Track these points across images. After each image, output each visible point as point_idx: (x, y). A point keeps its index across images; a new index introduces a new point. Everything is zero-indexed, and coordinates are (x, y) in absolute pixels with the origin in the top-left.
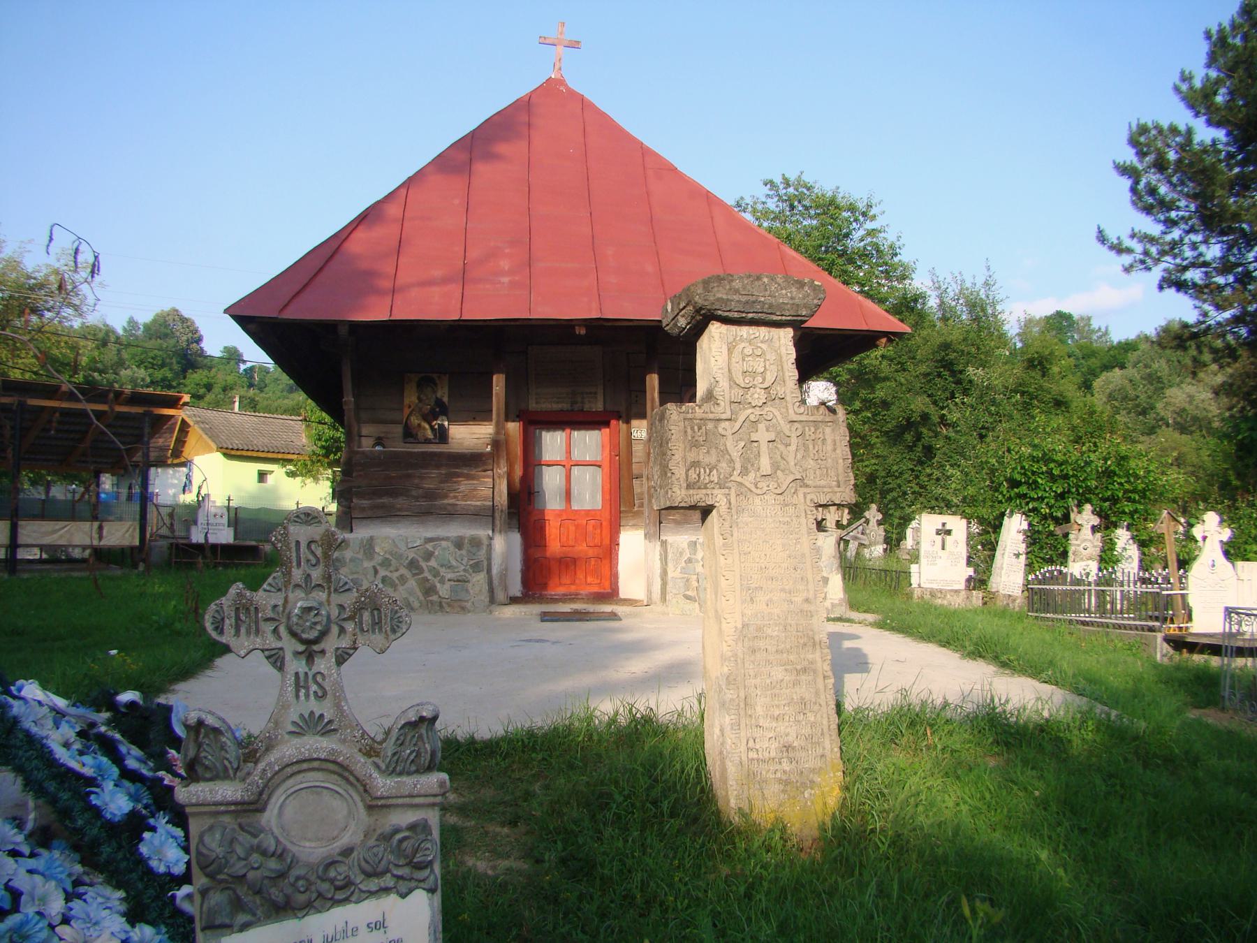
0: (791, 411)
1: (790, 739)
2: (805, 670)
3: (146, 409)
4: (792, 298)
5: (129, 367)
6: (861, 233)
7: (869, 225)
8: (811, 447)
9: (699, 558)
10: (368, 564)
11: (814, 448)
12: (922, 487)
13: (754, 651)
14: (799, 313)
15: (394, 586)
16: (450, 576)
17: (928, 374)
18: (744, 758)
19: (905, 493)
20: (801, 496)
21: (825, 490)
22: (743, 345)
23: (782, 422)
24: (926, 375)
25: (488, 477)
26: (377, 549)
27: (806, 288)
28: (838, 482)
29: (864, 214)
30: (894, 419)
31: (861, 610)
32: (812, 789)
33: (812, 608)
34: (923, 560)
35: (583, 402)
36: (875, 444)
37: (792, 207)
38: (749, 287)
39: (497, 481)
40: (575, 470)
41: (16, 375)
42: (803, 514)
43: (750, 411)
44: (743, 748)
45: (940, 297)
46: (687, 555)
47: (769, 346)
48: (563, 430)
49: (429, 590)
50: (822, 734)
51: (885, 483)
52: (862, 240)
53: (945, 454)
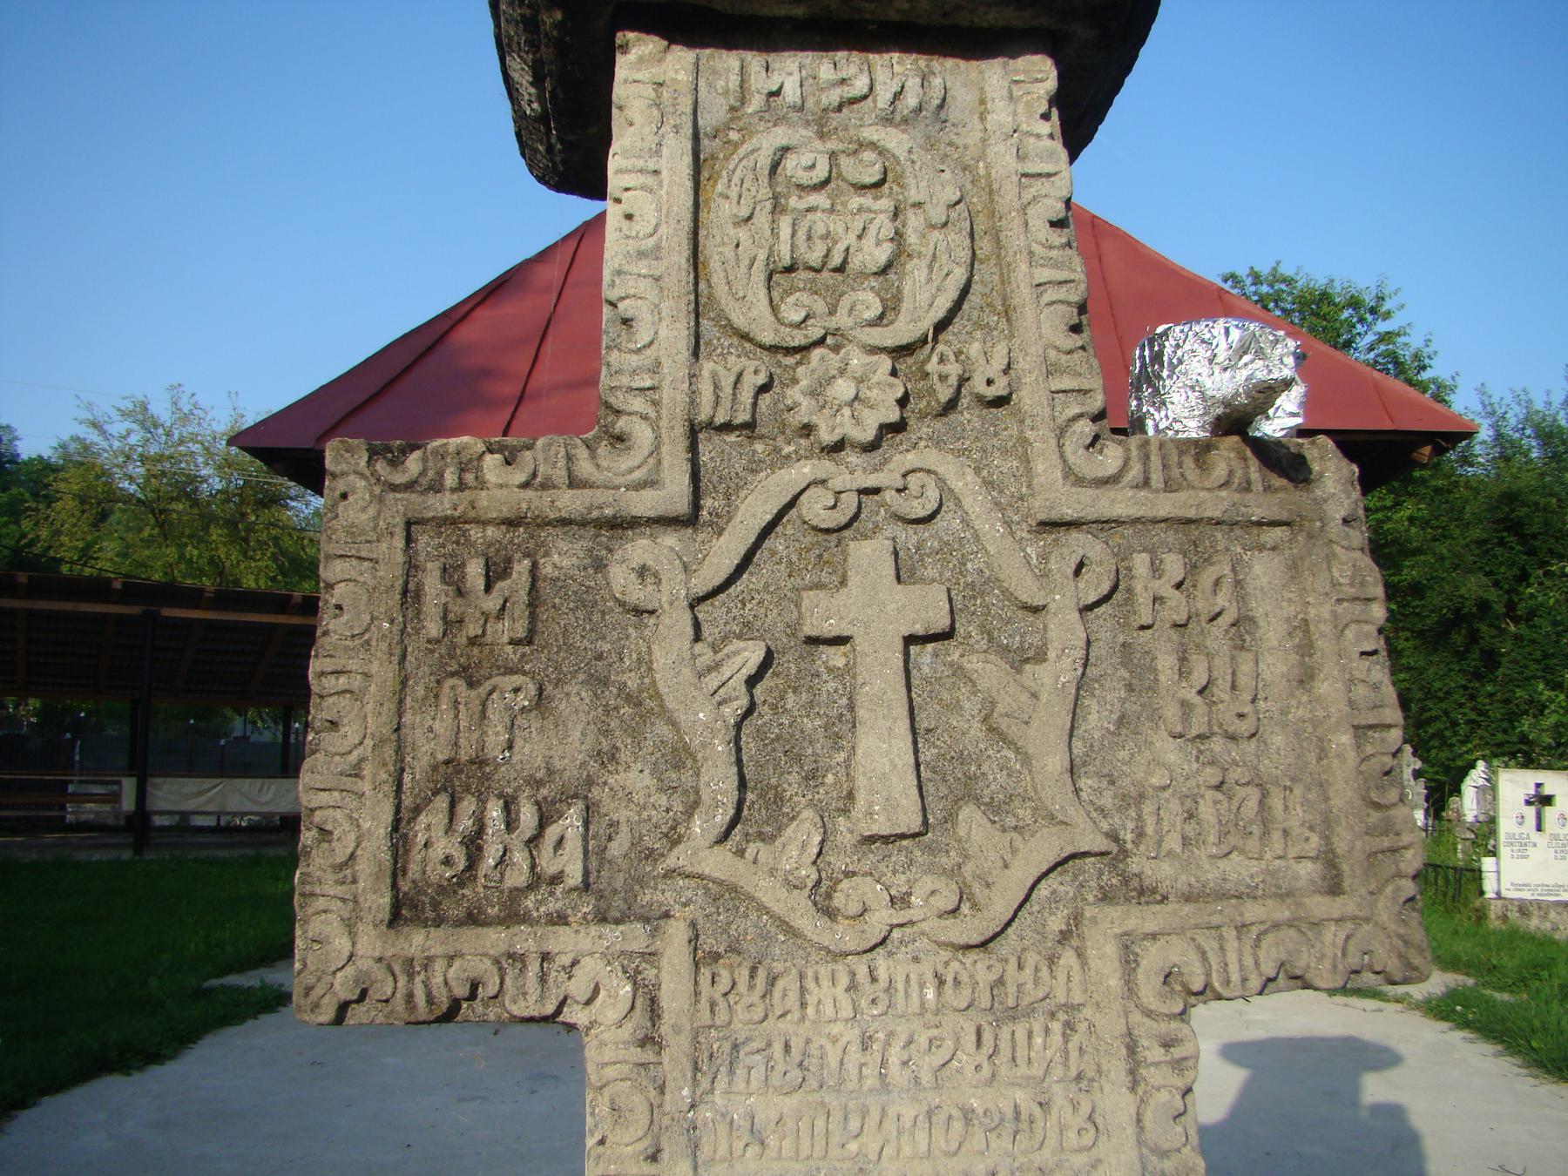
0: (1046, 469)
6: (1370, 338)
7: (1382, 327)
8: (1166, 663)
11: (1183, 672)
12: (1481, 713)
17: (1484, 542)
19: (1455, 724)
22: (781, 136)
23: (991, 528)
24: (1481, 543)
28: (1329, 860)
29: (1373, 311)
30: (1433, 611)
34: (1504, 851)
36: (1403, 649)
41: (249, 583)
42: (1117, 1068)
43: (806, 470)
45: (1495, 426)
51: (1423, 710)
52: (1371, 349)
53: (1515, 662)
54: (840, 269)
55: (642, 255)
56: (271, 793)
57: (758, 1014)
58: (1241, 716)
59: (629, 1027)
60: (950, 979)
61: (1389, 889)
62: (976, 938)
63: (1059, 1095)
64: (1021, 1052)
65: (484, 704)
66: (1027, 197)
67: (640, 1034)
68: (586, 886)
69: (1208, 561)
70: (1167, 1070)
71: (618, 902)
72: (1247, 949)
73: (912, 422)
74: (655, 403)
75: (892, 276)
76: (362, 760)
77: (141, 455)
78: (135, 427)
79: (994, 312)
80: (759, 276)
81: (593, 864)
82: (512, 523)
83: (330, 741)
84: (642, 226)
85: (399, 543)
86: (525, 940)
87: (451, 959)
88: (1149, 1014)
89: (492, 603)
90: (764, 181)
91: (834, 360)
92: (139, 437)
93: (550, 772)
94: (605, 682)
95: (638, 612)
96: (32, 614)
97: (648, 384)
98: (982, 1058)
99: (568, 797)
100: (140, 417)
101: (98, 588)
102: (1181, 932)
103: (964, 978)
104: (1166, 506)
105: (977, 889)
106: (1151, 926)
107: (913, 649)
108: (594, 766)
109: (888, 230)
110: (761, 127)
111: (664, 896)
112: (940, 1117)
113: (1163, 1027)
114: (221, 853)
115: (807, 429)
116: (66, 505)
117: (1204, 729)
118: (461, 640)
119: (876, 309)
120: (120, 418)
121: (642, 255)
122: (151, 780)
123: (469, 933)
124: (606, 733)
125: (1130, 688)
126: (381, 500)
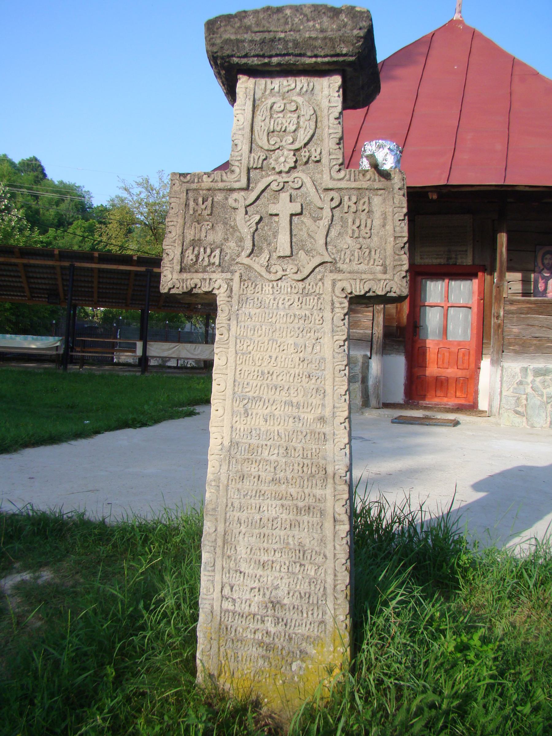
0: (326, 177)
2: (309, 509)
4: (322, 31)
9: (529, 381)
14: (338, 51)
18: (216, 608)
20: (328, 283)
21: (364, 276)
22: (273, 100)
23: (312, 190)
25: (369, 312)
27: (343, 17)
28: (384, 266)
32: (303, 661)
33: (327, 429)
35: (456, 258)
38: (264, 22)
39: (376, 315)
40: (451, 311)
42: (329, 307)
44: (217, 595)
46: (519, 378)
48: (443, 280)
50: (325, 594)
54: (285, 131)
55: (240, 129)
56: (199, 350)
57: (252, 292)
58: (367, 233)
59: (226, 293)
60: (293, 287)
61: (398, 273)
62: (300, 279)
63: (315, 313)
64: (308, 303)
65: (201, 228)
66: (330, 112)
67: (228, 295)
68: (219, 265)
69: (363, 198)
70: (340, 309)
71: (226, 269)
72: (362, 284)
73: (298, 167)
74: (241, 163)
75: (296, 133)
76: (176, 239)
77: (146, 203)
78: (144, 190)
79: (320, 140)
80: (266, 133)
81: (221, 261)
82: (209, 190)
83: (169, 235)
84: (240, 123)
85: (185, 194)
86: (206, 276)
87: (192, 279)
88: (338, 297)
89: (204, 207)
90: (269, 111)
91: (281, 153)
92: (145, 195)
93: (214, 242)
94: (227, 224)
95: (234, 209)
96: (100, 271)
97: (239, 159)
98: (299, 304)
99: (217, 247)
100: (145, 185)
101: (127, 260)
102: (347, 280)
103: (297, 287)
104: (354, 185)
105: (301, 268)
106: (340, 278)
107: (293, 217)
108: (223, 241)
109: (296, 122)
110: (269, 97)
111: (236, 268)
112: (289, 316)
113: (340, 300)
114: (178, 375)
115: (274, 169)
116: (114, 225)
117: (357, 236)
118: (197, 215)
119: (291, 140)
120: (136, 186)
121: (240, 129)
122: (149, 343)
123: (195, 274)
124: (227, 234)
125: (342, 226)
126: (181, 185)
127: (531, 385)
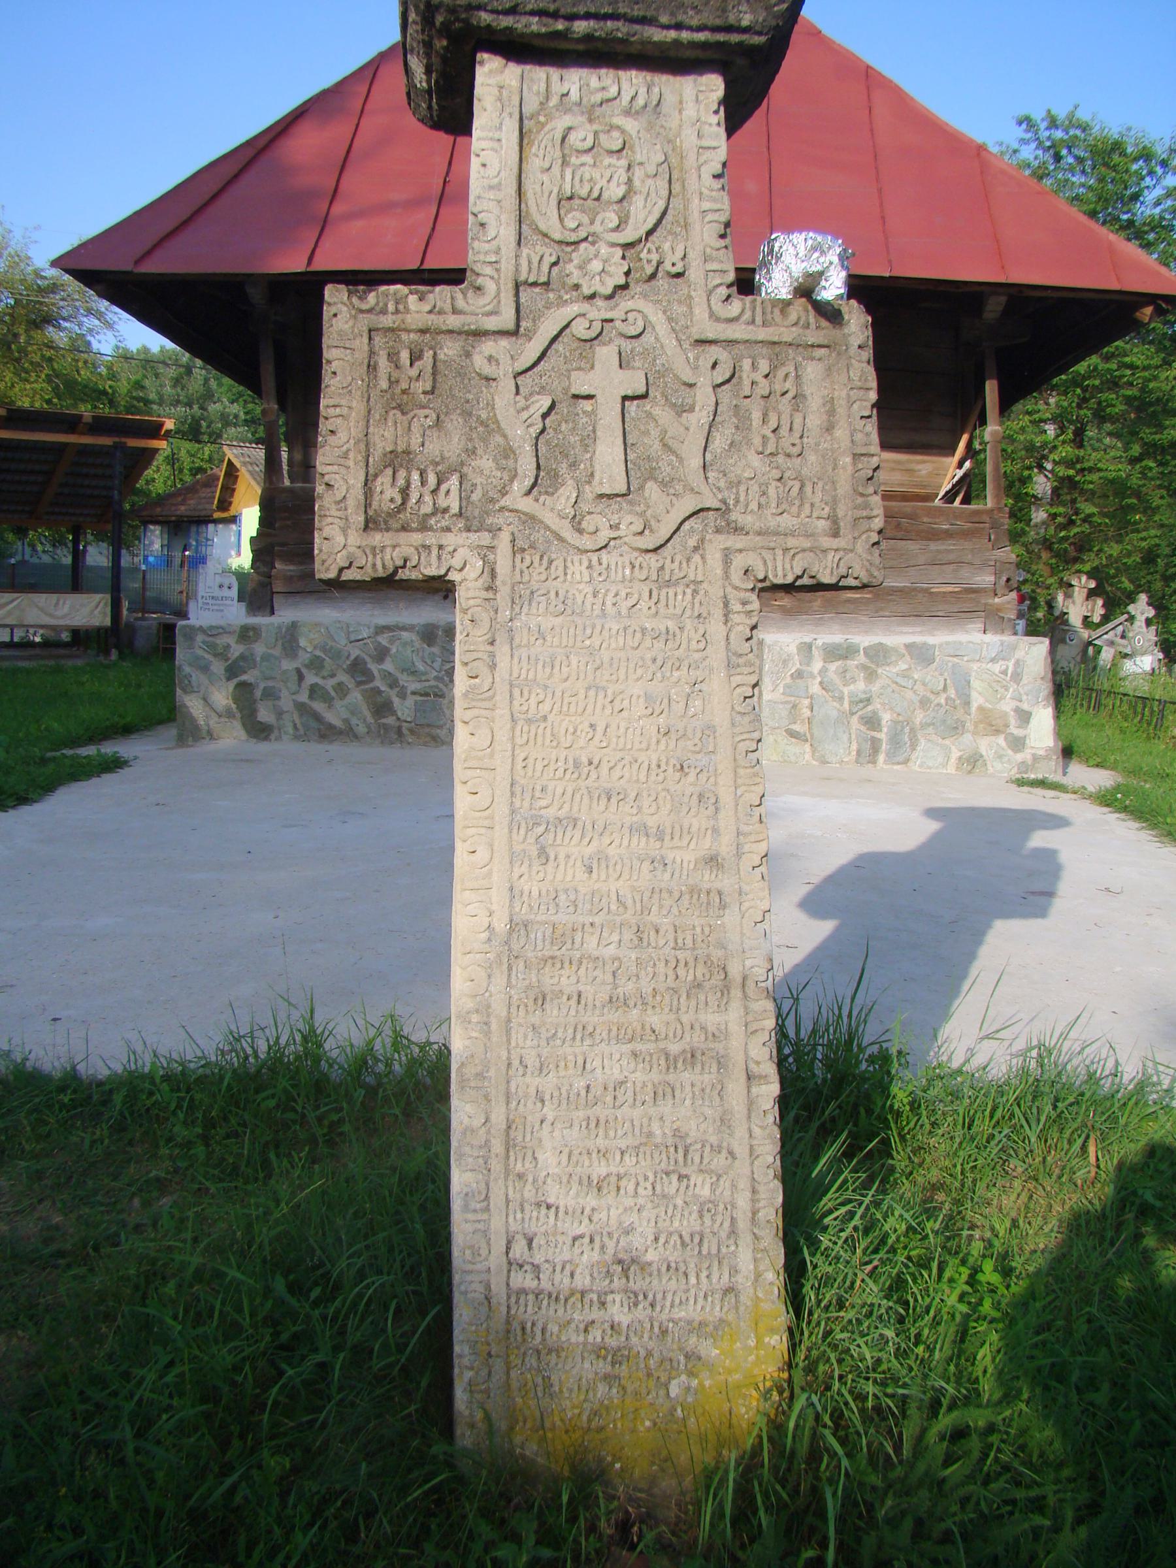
1: (636, 1241)
3: (117, 440)
5: (219, 400)
6: (1158, 192)
9: (816, 671)
10: (288, 665)
11: (764, 421)
13: (541, 999)
14: (732, 19)
15: (328, 700)
16: (414, 686)
21: (791, 542)
22: (567, 121)
23: (670, 343)
26: (303, 642)
28: (834, 520)
29: (1164, 164)
31: (1092, 762)
32: (691, 1374)
33: (726, 882)
36: (1158, 507)
37: (1058, 158)
41: (25, 403)
42: (718, 613)
47: (650, 127)
49: (382, 708)
50: (733, 1232)
127: (819, 679)
